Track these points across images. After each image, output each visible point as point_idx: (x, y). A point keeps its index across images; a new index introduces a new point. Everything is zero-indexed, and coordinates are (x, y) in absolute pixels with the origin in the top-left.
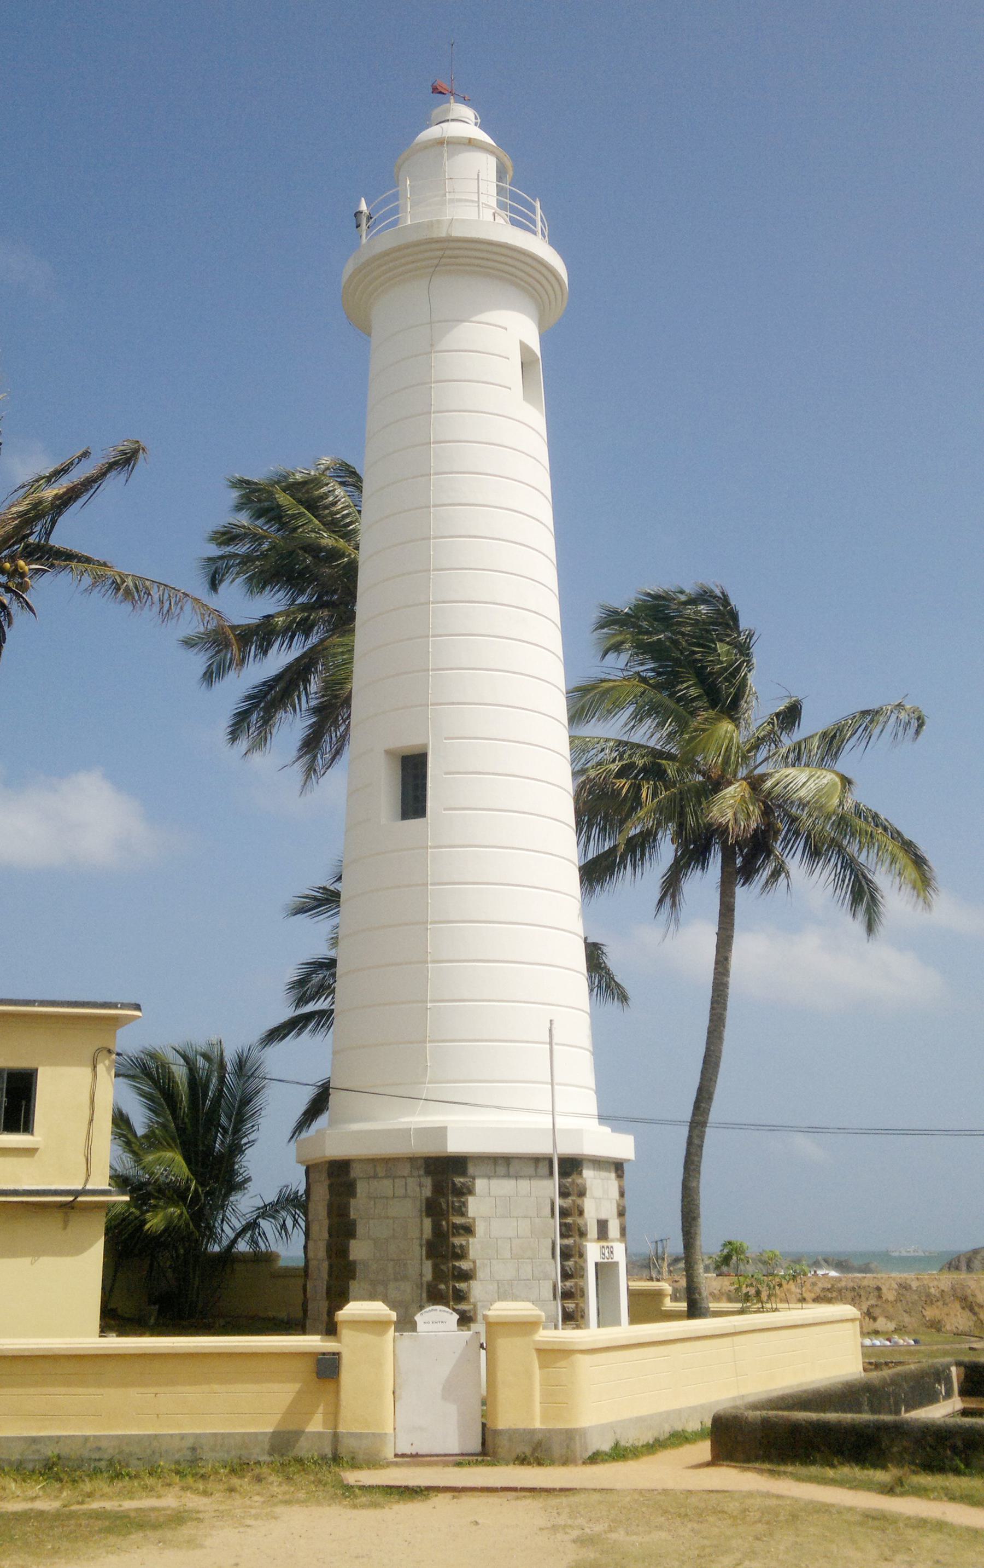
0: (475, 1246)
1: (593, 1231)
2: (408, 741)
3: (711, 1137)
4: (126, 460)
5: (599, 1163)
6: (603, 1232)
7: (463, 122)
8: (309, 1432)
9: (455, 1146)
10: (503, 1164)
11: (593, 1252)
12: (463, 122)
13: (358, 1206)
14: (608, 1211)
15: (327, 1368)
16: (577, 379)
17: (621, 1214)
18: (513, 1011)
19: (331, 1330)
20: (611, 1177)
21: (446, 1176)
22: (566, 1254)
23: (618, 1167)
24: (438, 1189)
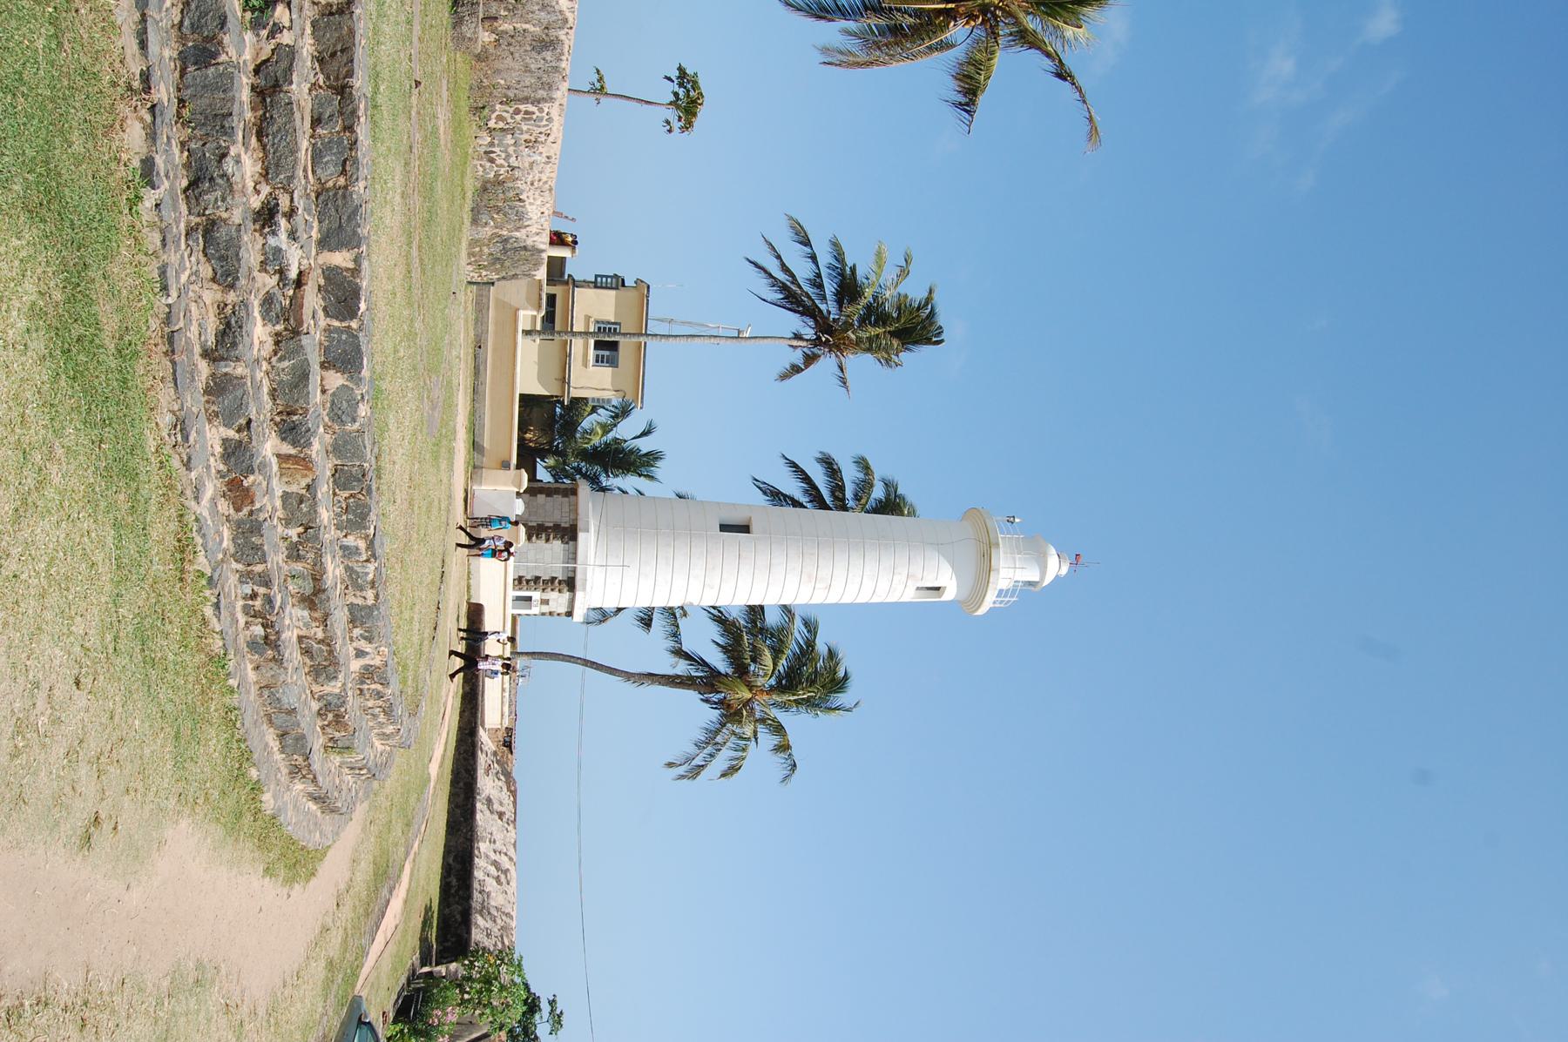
0: (541, 543)
1: (546, 596)
2: (753, 528)
3: (579, 668)
4: (844, 382)
5: (572, 602)
6: (545, 602)
7: (1056, 567)
8: (616, 314)
9: (581, 536)
10: (573, 557)
11: (536, 595)
12: (1056, 567)
13: (558, 498)
14: (553, 607)
15: (505, 465)
16: (926, 613)
17: (551, 614)
18: (636, 571)
19: (518, 467)
20: (563, 610)
21: (569, 533)
22: (537, 579)
23: (569, 614)
24: (565, 529)
